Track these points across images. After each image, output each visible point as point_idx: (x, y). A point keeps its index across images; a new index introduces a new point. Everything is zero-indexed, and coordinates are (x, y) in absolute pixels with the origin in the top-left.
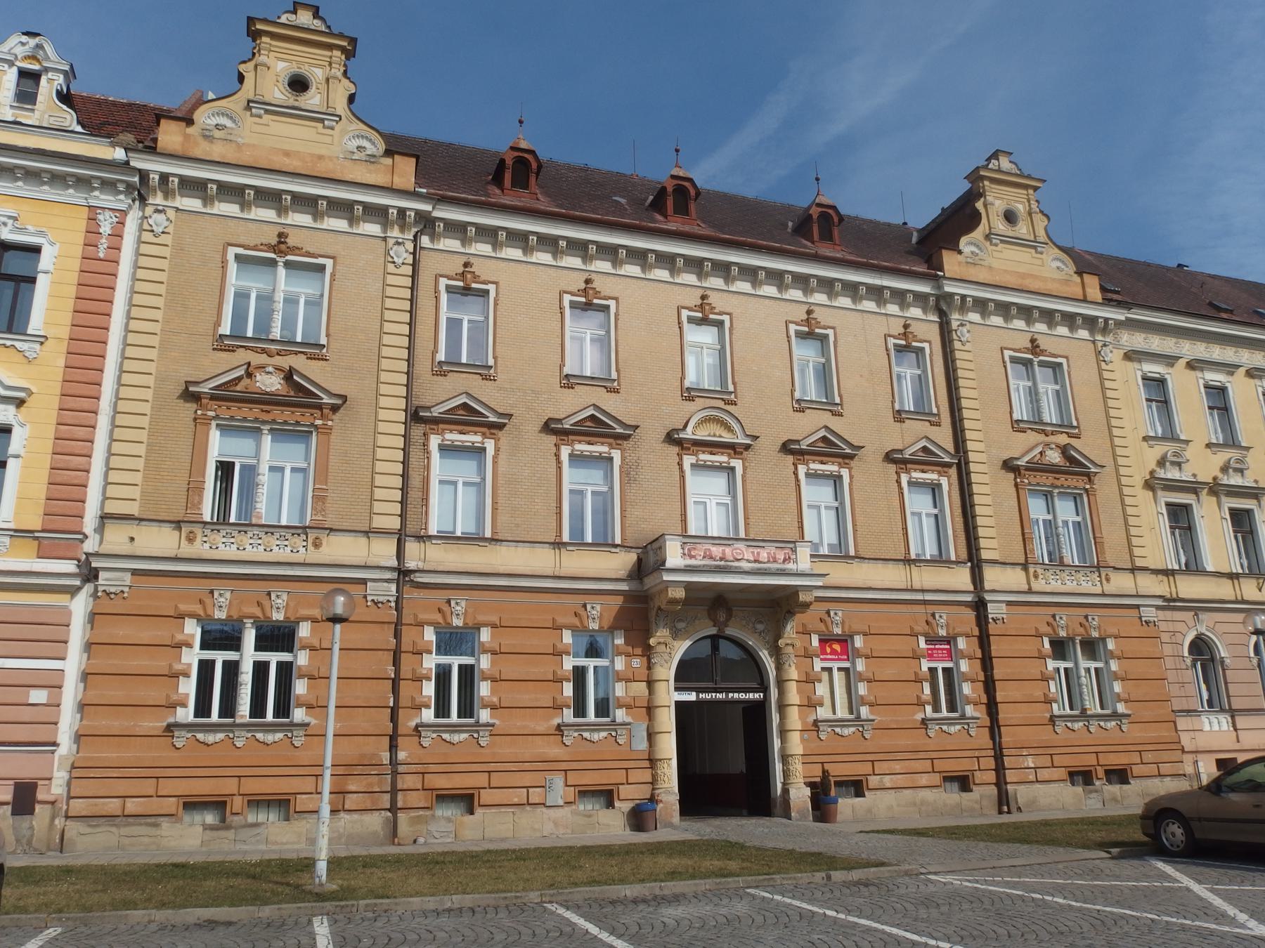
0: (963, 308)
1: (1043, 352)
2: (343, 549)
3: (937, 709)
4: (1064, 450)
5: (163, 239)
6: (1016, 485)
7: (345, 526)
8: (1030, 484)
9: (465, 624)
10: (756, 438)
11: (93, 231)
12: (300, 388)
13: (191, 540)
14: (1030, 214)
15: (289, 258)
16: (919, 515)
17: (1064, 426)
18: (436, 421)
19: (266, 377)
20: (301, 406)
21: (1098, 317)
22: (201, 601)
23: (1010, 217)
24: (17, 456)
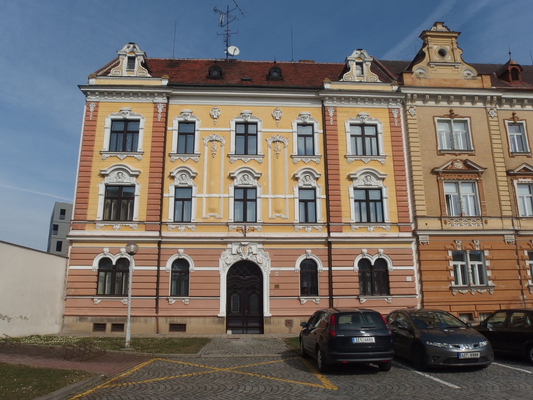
0: (412, 99)
1: (456, 116)
2: (494, 224)
3: (457, 283)
4: (465, 162)
5: (414, 117)
6: (437, 181)
7: (493, 215)
8: (445, 179)
9: (462, 249)
10: (486, 169)
11: (391, 117)
12: (469, 167)
13: (446, 223)
14: (453, 50)
15: (455, 119)
16: (523, 197)
17: (469, 151)
18: (515, 175)
19: (457, 163)
20: (470, 172)
21: (487, 96)
22: (452, 245)
23: (442, 53)
24: (386, 198)
